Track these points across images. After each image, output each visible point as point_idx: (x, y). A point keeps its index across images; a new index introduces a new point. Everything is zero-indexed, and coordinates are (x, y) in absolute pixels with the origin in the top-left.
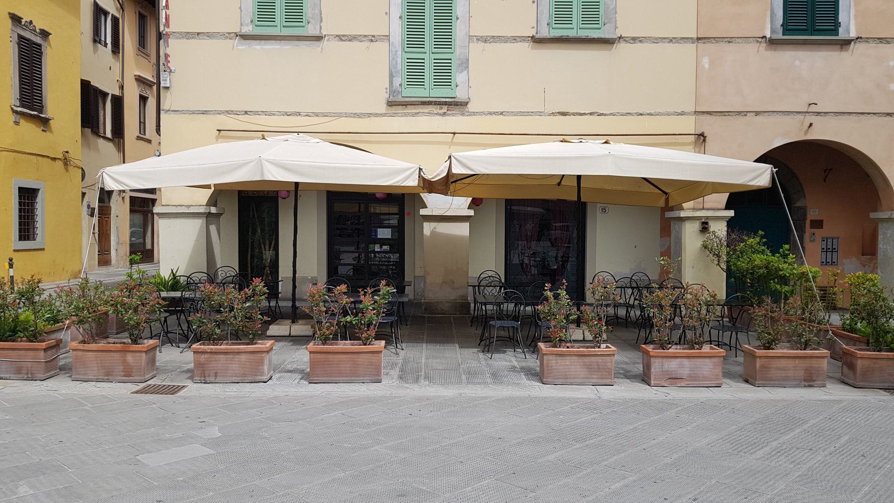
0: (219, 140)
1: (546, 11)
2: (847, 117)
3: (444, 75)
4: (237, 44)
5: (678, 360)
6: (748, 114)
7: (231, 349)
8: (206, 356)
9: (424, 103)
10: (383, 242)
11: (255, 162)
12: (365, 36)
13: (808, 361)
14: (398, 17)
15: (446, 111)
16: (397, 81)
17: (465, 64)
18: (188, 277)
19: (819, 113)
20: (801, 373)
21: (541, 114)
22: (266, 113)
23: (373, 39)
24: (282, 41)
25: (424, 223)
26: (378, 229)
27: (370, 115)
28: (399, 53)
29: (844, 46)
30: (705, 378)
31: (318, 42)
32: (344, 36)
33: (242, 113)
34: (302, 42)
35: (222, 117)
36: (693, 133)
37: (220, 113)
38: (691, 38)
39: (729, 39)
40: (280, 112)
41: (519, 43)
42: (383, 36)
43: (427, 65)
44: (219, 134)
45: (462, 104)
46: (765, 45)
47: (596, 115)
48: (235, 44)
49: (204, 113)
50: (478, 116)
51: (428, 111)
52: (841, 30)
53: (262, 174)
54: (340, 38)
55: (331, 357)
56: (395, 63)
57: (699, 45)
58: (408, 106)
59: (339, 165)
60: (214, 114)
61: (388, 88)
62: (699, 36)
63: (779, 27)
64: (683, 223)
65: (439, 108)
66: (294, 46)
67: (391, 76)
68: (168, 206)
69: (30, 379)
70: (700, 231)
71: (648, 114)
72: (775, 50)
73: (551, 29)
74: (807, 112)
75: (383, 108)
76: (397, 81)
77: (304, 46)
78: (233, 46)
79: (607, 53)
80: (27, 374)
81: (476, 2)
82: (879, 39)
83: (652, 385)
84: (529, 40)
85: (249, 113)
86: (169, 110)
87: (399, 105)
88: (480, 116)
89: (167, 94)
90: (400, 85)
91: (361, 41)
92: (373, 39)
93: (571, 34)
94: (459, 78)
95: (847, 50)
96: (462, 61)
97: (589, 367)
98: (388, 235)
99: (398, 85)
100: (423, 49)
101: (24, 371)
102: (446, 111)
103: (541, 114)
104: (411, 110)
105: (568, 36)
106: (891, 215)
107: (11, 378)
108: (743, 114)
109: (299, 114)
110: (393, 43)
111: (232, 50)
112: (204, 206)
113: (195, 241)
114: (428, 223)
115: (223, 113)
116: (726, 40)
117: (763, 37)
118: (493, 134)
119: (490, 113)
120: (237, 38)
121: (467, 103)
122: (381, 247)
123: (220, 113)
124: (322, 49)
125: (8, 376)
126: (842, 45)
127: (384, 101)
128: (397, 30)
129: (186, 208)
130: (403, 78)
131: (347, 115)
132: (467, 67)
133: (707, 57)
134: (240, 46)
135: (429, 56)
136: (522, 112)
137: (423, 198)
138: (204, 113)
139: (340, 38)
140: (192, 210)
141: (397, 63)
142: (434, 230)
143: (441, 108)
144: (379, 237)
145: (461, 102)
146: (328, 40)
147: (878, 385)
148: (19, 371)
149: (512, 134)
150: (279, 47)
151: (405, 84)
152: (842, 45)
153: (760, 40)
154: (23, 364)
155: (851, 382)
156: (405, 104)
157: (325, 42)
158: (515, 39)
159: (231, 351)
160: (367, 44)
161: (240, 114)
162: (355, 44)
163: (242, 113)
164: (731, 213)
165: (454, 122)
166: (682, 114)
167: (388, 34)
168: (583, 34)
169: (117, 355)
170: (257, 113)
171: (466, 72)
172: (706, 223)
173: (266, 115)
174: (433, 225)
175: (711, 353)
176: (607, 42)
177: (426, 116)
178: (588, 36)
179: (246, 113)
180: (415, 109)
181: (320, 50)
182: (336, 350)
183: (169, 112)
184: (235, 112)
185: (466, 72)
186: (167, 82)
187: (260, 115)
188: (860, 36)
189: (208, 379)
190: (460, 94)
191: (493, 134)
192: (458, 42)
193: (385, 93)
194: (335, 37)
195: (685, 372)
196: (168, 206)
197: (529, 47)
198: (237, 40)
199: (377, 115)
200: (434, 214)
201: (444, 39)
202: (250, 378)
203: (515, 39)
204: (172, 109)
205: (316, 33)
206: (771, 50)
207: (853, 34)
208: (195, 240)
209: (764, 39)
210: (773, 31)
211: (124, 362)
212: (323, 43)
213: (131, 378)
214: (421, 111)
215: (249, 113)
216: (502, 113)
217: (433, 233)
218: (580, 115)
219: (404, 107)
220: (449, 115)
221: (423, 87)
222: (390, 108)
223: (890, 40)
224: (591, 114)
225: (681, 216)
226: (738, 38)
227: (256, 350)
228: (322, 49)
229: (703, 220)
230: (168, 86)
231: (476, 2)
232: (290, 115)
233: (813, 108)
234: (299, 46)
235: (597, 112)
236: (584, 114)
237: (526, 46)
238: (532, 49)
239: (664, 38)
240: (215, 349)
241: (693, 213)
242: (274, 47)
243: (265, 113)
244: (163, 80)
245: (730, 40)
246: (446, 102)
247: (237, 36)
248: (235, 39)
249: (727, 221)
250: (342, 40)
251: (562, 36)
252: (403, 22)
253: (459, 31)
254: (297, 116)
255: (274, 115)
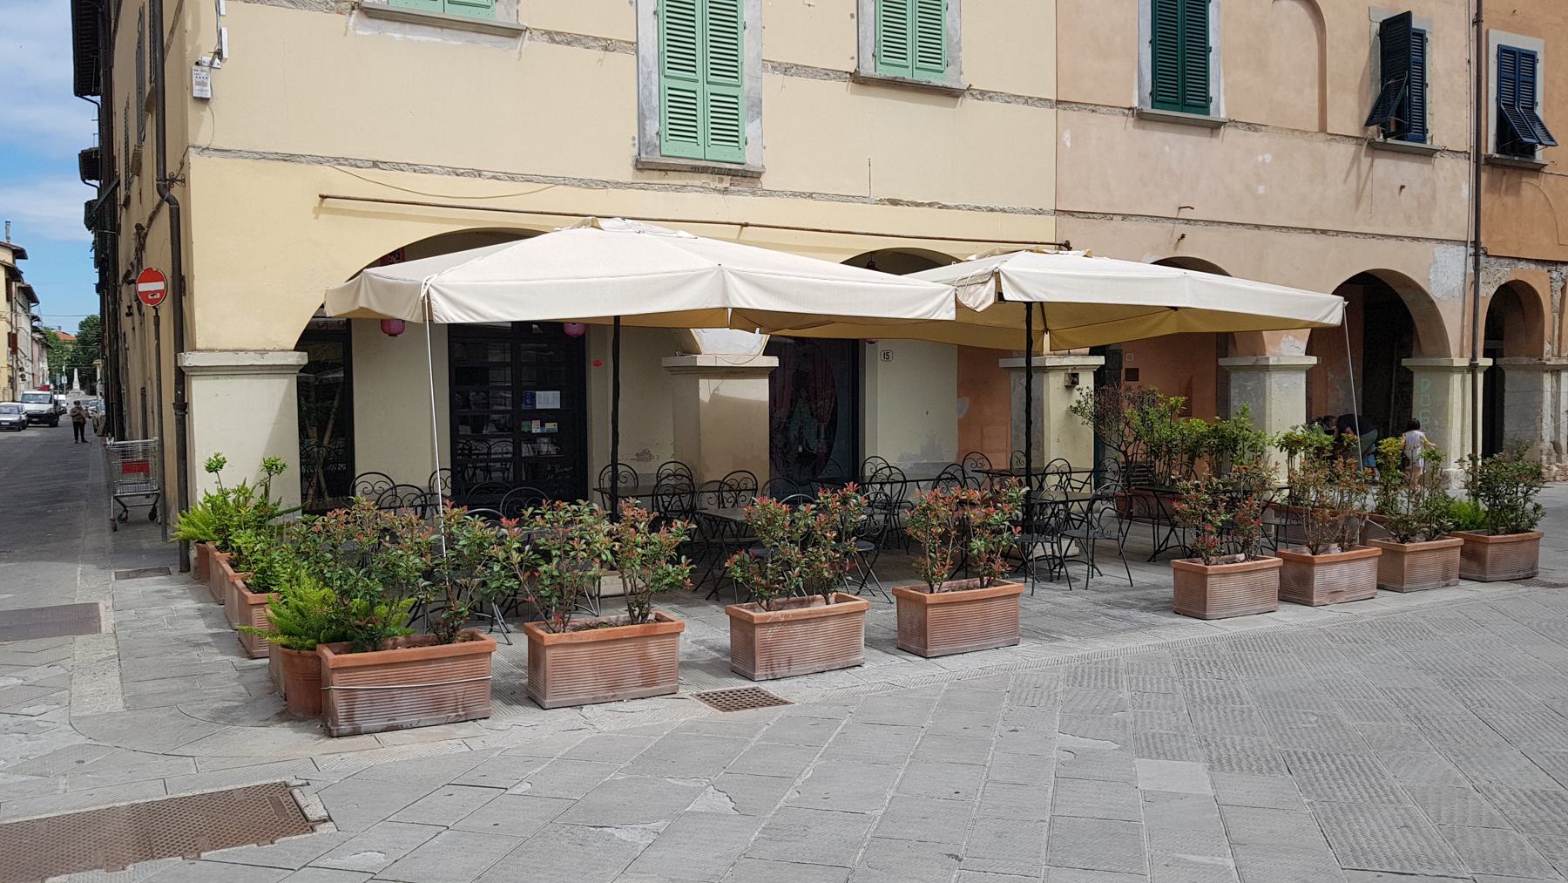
0: (322, 216)
1: (870, 34)
2: (1216, 227)
3: (727, 124)
4: (355, 24)
5: (1339, 567)
6: (1115, 217)
7: (802, 615)
8: (776, 629)
9: (696, 170)
10: (545, 416)
11: (713, 274)
12: (596, 39)
13: (1445, 553)
14: (652, 13)
15: (728, 185)
16: (653, 127)
17: (756, 107)
18: (721, 483)
19: (1189, 220)
20: (1439, 570)
21: (866, 200)
22: (416, 168)
23: (608, 46)
24: (446, 31)
25: (700, 380)
26: (537, 393)
27: (605, 184)
28: (655, 76)
29: (1214, 131)
30: (1363, 589)
31: (512, 40)
32: (558, 33)
33: (368, 164)
34: (483, 36)
35: (327, 170)
36: (1053, 241)
37: (321, 161)
38: (1050, 100)
39: (1093, 107)
40: (443, 167)
41: (832, 81)
42: (626, 42)
43: (699, 102)
44: (322, 202)
45: (755, 175)
46: (1131, 119)
47: (936, 206)
48: (351, 24)
49: (288, 158)
50: (776, 198)
51: (699, 184)
52: (1212, 107)
53: (726, 296)
54: (552, 36)
55: (954, 609)
56: (648, 93)
57: (1059, 111)
58: (669, 173)
59: (870, 284)
60: (308, 163)
61: (637, 137)
62: (1059, 99)
63: (1148, 95)
64: (1045, 375)
65: (717, 179)
66: (467, 41)
67: (641, 118)
68: (212, 350)
69: (463, 719)
70: (1066, 386)
71: (1001, 210)
72: (1144, 128)
73: (878, 63)
74: (1176, 219)
75: (627, 173)
76: (653, 127)
77: (486, 43)
78: (347, 28)
79: (949, 110)
80: (456, 710)
81: (770, 3)
82: (1248, 124)
83: (1315, 604)
84: (846, 78)
85: (381, 166)
86: (208, 148)
87: (654, 170)
88: (779, 198)
89: (202, 113)
90: (657, 134)
91: (588, 48)
92: (608, 46)
93: (906, 74)
94: (749, 129)
95: (1217, 136)
96: (753, 102)
97: (1252, 587)
98: (554, 403)
99: (654, 133)
100: (694, 74)
101: (449, 705)
102: (728, 185)
103: (866, 200)
104: (675, 179)
105: (904, 78)
106: (1257, 360)
107: (420, 724)
108: (1108, 216)
109: (479, 174)
110: (643, 57)
111: (345, 35)
112: (291, 350)
113: (274, 424)
114: (707, 381)
115: (328, 161)
116: (1090, 107)
117: (1129, 109)
118: (804, 229)
119: (794, 194)
120: (355, 12)
121: (760, 174)
122: (542, 425)
123: (321, 161)
124: (520, 53)
125: (414, 720)
126: (1212, 129)
127: (630, 161)
128: (650, 37)
129: (258, 356)
130: (663, 123)
131: (566, 182)
132: (760, 113)
133: (1068, 131)
134: (359, 30)
135: (703, 88)
136: (840, 195)
137: (695, 337)
138: (288, 158)
139: (552, 36)
140: (269, 360)
141: (650, 94)
142: (716, 392)
143: (721, 181)
144: (538, 407)
145: (753, 172)
146: (531, 39)
147: (1504, 576)
148: (437, 706)
149: (830, 231)
150: (439, 40)
151: (666, 133)
152: (1212, 129)
153: (1126, 111)
154: (447, 689)
155: (1474, 576)
156: (665, 169)
157: (525, 42)
158: (828, 74)
159: (816, 616)
160: (597, 53)
161: (362, 165)
162: (577, 50)
163: (368, 164)
164: (1313, 360)
165: (740, 205)
166: (1040, 212)
167: (635, 40)
168: (922, 77)
169: (629, 647)
170: (396, 166)
171: (759, 120)
172: (1075, 376)
173: (415, 171)
174: (715, 383)
175: (1342, 556)
176: (951, 93)
177: (697, 191)
178: (929, 82)
179: (375, 164)
180: (680, 178)
181: (518, 56)
182: (964, 597)
183: (207, 152)
184: (353, 163)
185: (759, 120)
186: (206, 88)
187: (402, 170)
188: (1232, 119)
189: (779, 672)
190: (751, 159)
191: (804, 229)
192: (745, 71)
193: (631, 147)
194: (543, 34)
195: (1344, 583)
196: (212, 350)
197: (847, 90)
198: (353, 16)
199: (617, 185)
200: (718, 365)
201: (727, 62)
202: (840, 662)
203: (828, 74)
204: (215, 145)
205: (510, 22)
206: (1139, 128)
207: (1223, 116)
208: (273, 421)
209: (1131, 112)
210: (1141, 101)
211: (644, 657)
212: (522, 44)
213: (655, 688)
214: (690, 183)
215: (381, 166)
216: (811, 196)
217: (715, 397)
218: (916, 206)
219: (663, 173)
220: (733, 193)
221: (736, 144)
222: (639, 173)
223: (1258, 127)
224: (930, 205)
225: (1047, 365)
226: (1103, 106)
227: (853, 610)
228: (520, 53)
229: (1070, 371)
230: (209, 96)
231: (770, 3)
232: (462, 174)
233: (1185, 214)
234: (477, 43)
235: (938, 203)
236: (922, 205)
237: (843, 88)
238: (851, 93)
239: (1019, 97)
240: (793, 615)
241: (1059, 360)
242: (428, 39)
243: (414, 168)
244: (198, 84)
245: (1094, 108)
246: (721, 169)
247: (353, 8)
248: (350, 15)
249: (1094, 372)
250: (553, 41)
251: (896, 78)
252: (661, 21)
253: (749, 49)
254: (475, 176)
255: (432, 172)
